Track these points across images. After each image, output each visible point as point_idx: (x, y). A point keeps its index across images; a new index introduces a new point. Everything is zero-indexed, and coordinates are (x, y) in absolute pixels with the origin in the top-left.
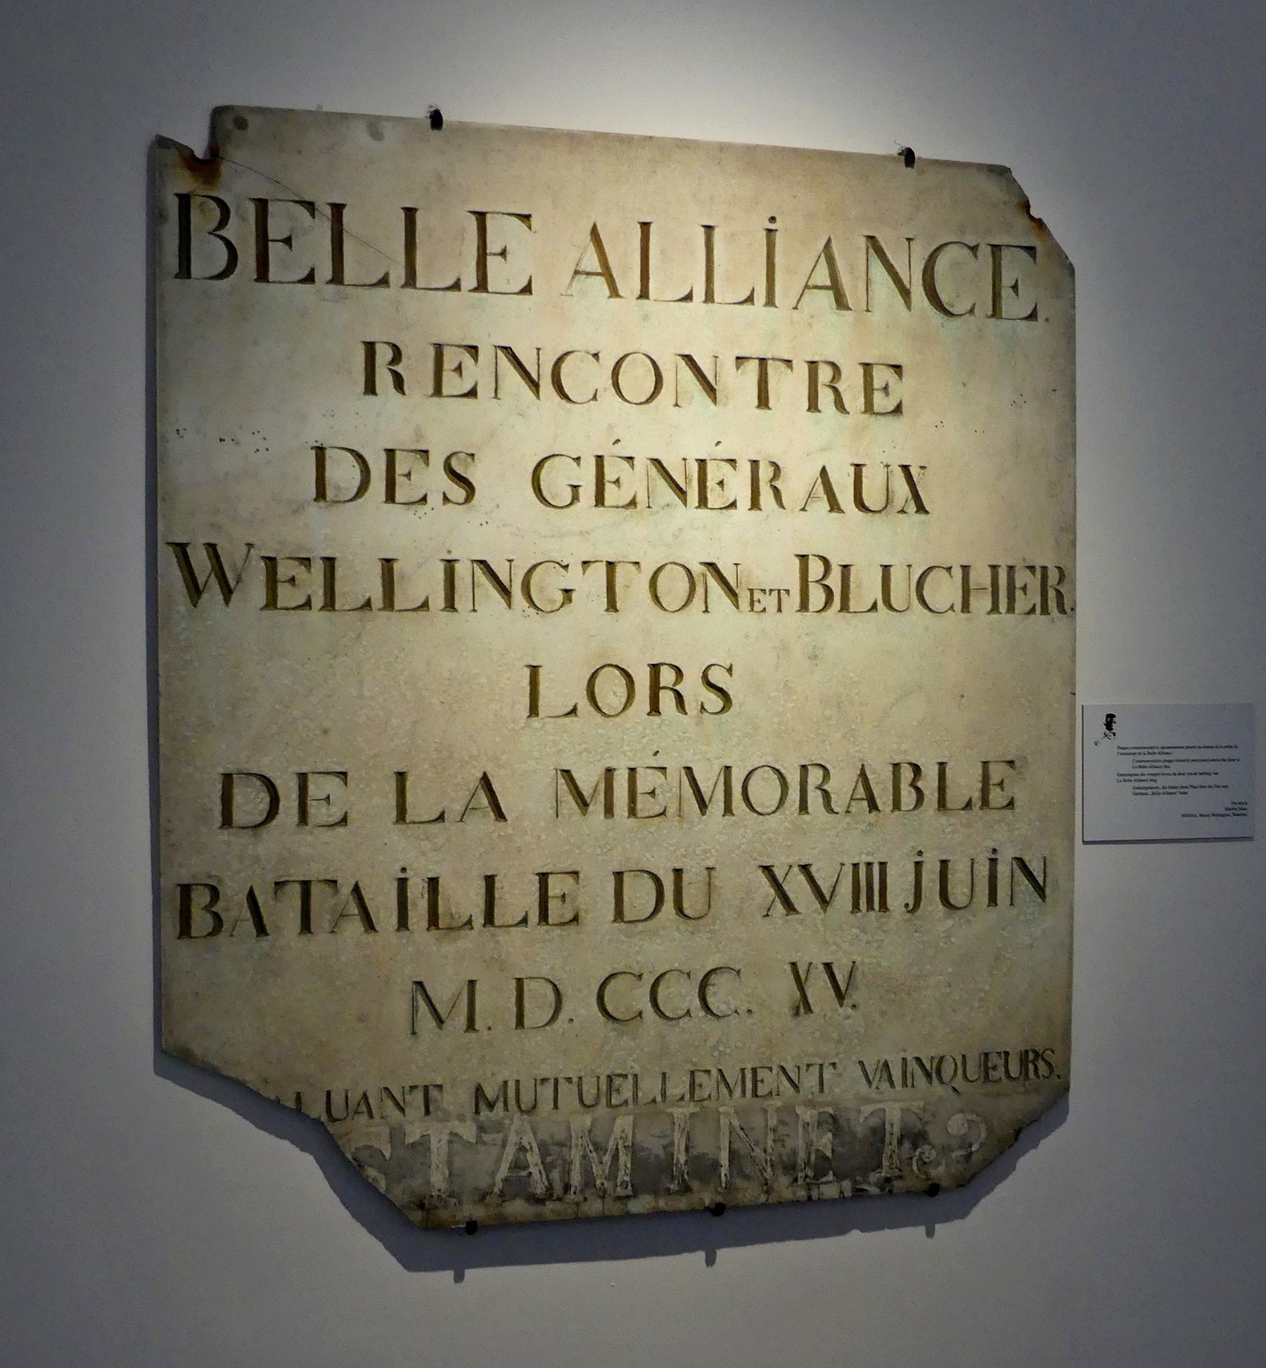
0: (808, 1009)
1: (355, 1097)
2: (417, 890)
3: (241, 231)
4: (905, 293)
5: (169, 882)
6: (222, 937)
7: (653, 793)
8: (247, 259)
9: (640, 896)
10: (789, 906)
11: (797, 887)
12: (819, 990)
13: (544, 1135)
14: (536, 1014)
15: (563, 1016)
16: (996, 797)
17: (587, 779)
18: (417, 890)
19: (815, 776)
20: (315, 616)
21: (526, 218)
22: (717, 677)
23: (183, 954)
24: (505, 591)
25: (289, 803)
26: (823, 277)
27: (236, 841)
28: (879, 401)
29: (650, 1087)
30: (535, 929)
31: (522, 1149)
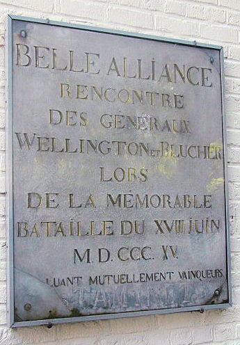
0: (167, 258)
1: (61, 280)
2: (75, 225)
3: (32, 54)
4: (183, 78)
5: (16, 223)
6: (28, 237)
7: (130, 201)
8: (33, 62)
9: (127, 227)
10: (161, 231)
11: (163, 226)
12: (169, 253)
13: (106, 291)
14: (104, 258)
15: (110, 259)
16: (208, 204)
17: (114, 197)
18: (75, 225)
19: (167, 198)
20: (50, 153)
21: (98, 55)
22: (144, 172)
23: (18, 240)
24: (94, 148)
25: (44, 202)
26: (165, 74)
27: (104, 265)
28: (178, 105)
29: (131, 278)
30: (137, 79)
31: (101, 294)
